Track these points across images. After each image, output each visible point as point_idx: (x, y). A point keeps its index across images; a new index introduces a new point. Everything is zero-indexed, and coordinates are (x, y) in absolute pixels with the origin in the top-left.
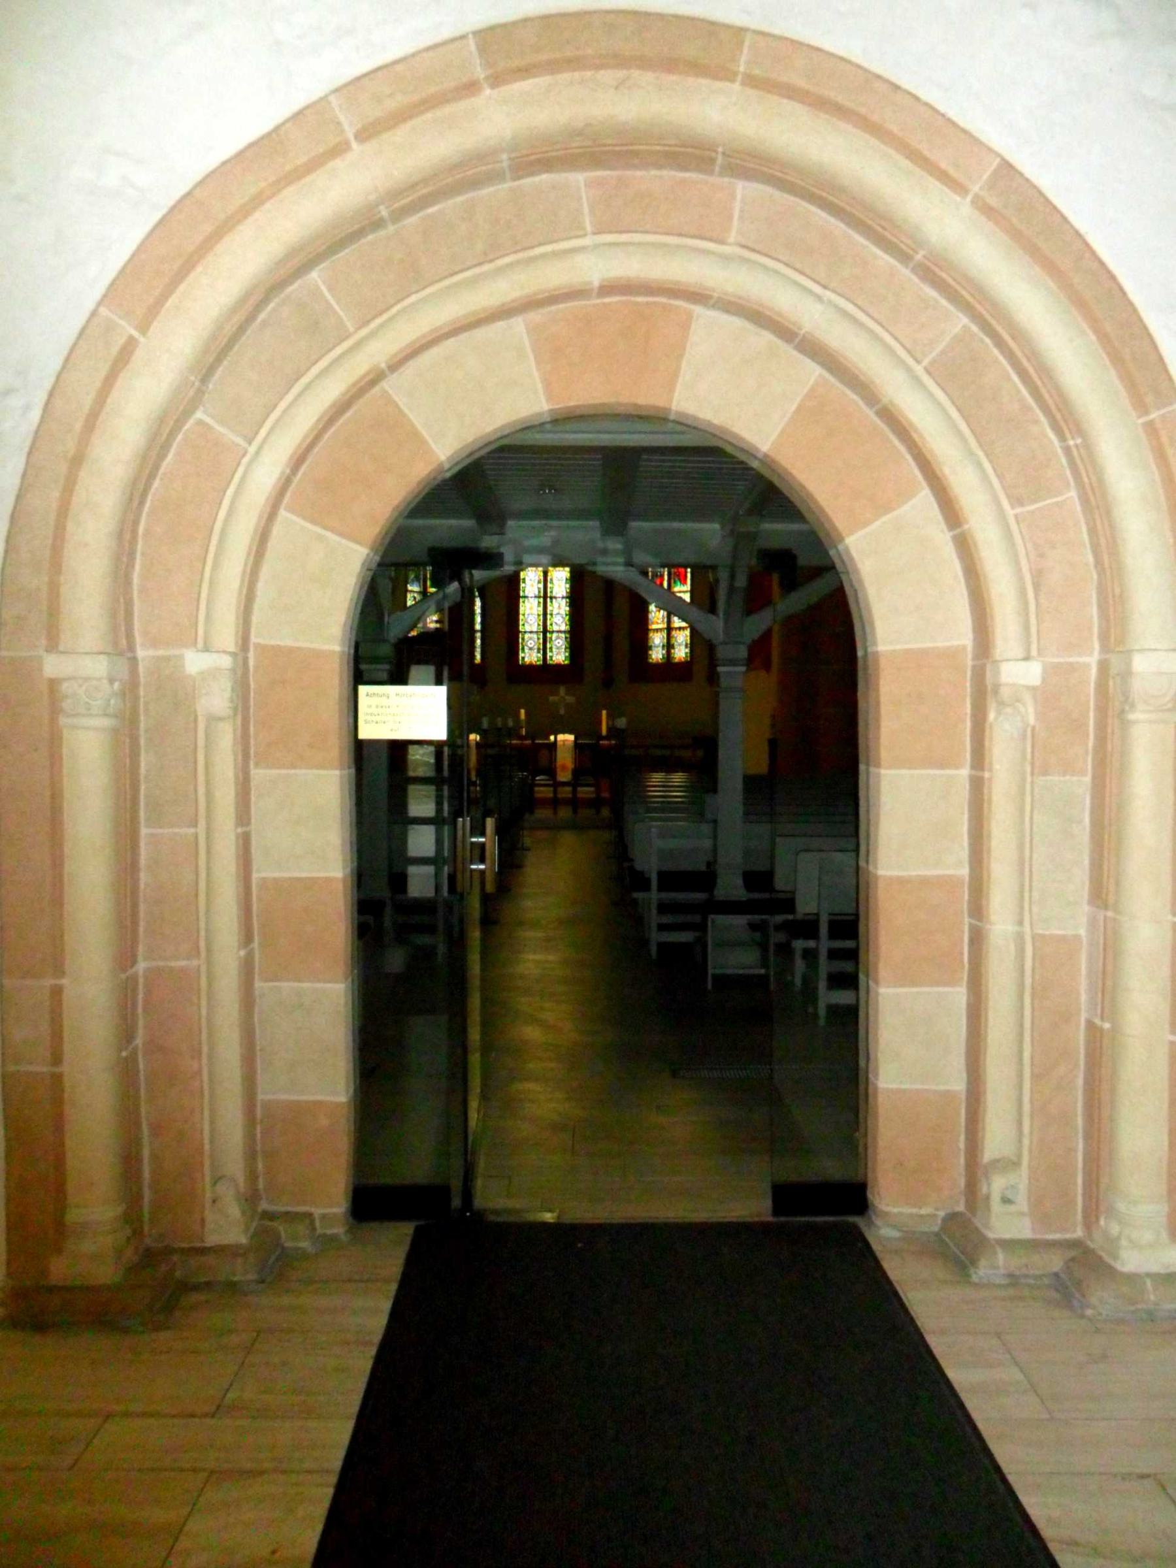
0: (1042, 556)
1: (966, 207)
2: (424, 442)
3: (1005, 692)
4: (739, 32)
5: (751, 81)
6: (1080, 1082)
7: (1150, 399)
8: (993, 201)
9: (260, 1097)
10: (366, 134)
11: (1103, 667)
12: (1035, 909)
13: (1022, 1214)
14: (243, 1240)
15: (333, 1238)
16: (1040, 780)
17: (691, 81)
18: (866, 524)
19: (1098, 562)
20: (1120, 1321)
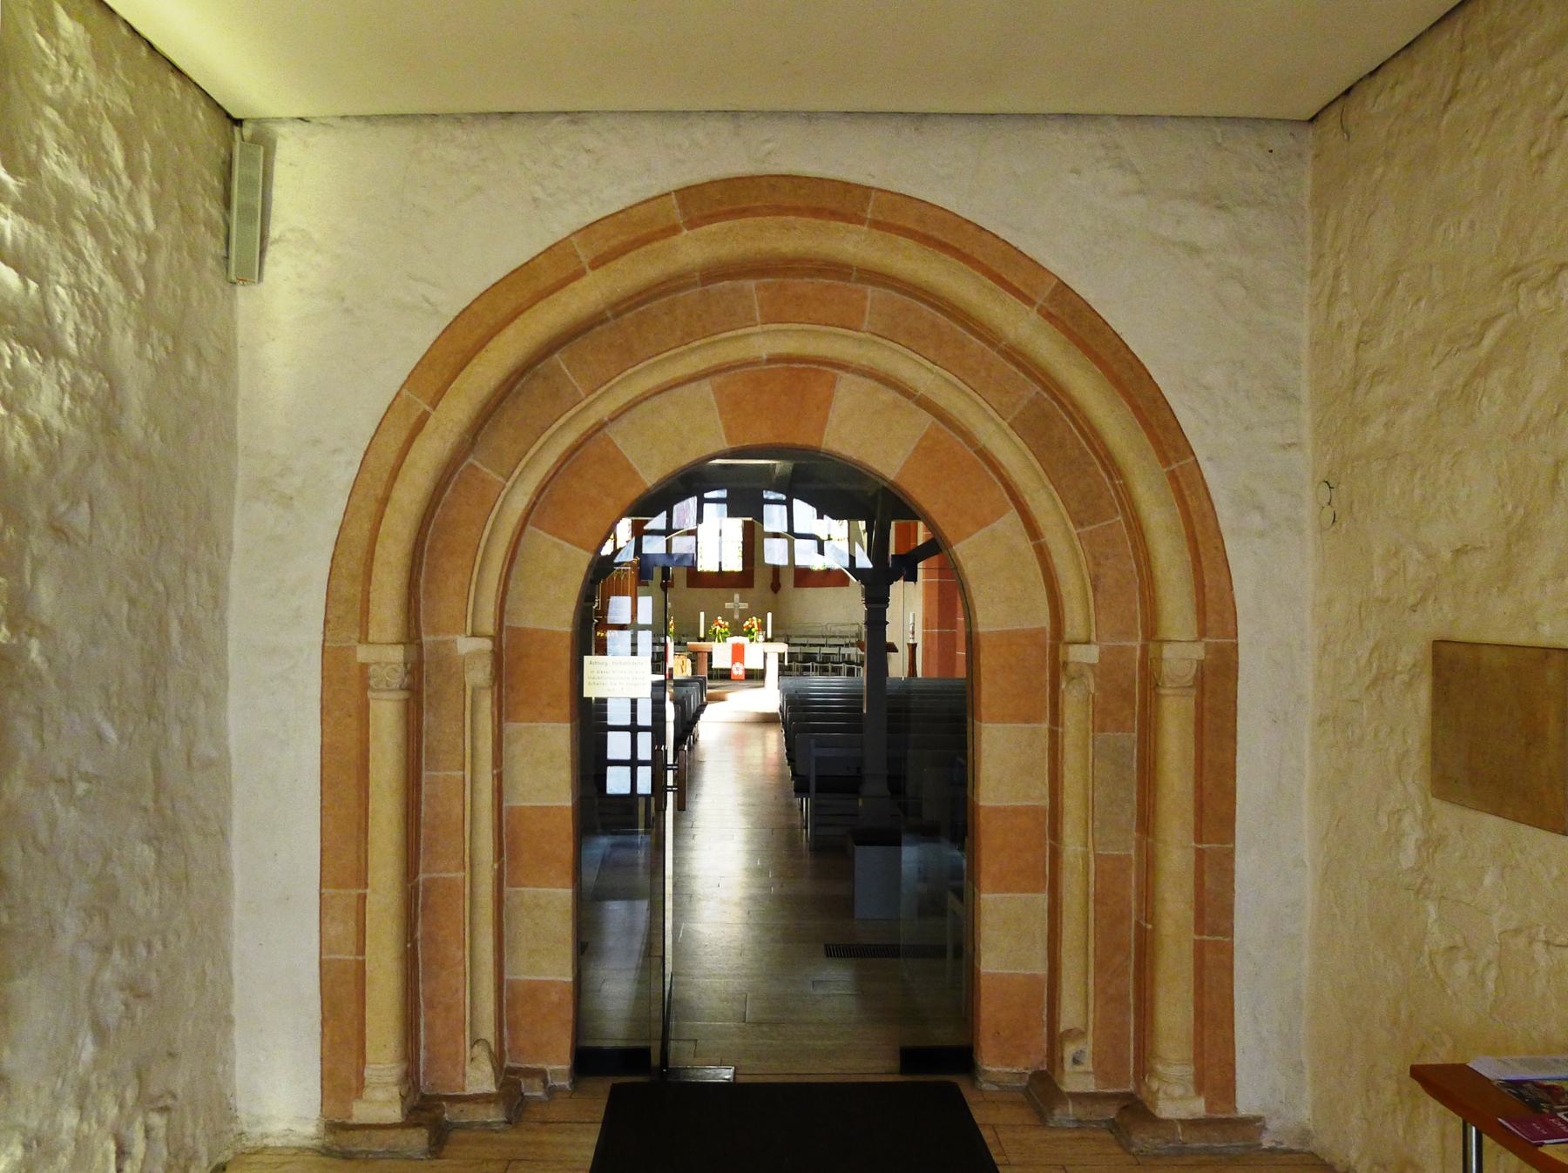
0: (1098, 564)
1: (1033, 314)
2: (635, 473)
3: (1072, 668)
4: (866, 190)
5: (876, 224)
6: (1131, 969)
7: (1171, 454)
8: (1053, 310)
9: (506, 977)
10: (598, 262)
11: (1144, 649)
12: (1097, 835)
13: (1086, 1073)
14: (494, 1090)
15: (562, 1089)
16: (1100, 736)
17: (834, 224)
18: (969, 535)
19: (1139, 570)
20: (1157, 1156)
